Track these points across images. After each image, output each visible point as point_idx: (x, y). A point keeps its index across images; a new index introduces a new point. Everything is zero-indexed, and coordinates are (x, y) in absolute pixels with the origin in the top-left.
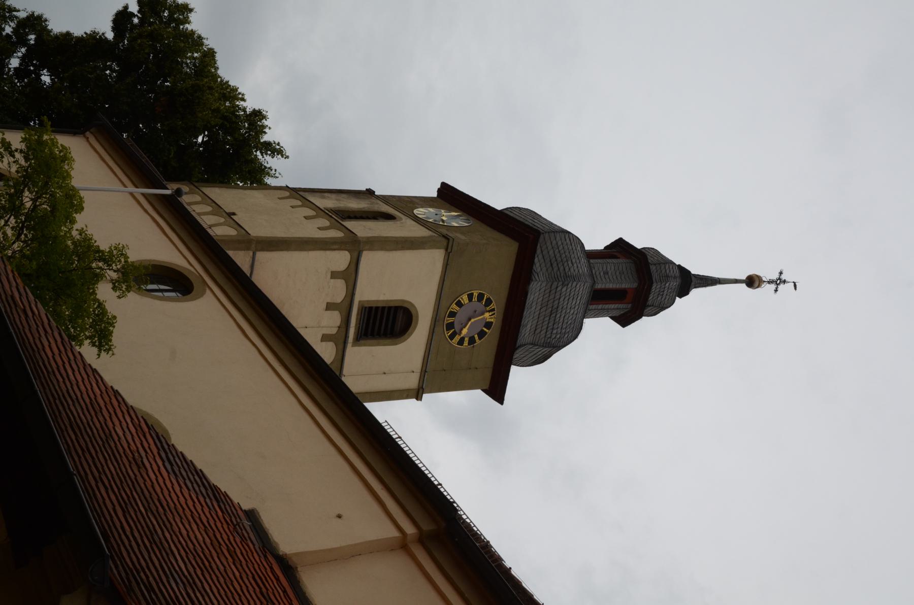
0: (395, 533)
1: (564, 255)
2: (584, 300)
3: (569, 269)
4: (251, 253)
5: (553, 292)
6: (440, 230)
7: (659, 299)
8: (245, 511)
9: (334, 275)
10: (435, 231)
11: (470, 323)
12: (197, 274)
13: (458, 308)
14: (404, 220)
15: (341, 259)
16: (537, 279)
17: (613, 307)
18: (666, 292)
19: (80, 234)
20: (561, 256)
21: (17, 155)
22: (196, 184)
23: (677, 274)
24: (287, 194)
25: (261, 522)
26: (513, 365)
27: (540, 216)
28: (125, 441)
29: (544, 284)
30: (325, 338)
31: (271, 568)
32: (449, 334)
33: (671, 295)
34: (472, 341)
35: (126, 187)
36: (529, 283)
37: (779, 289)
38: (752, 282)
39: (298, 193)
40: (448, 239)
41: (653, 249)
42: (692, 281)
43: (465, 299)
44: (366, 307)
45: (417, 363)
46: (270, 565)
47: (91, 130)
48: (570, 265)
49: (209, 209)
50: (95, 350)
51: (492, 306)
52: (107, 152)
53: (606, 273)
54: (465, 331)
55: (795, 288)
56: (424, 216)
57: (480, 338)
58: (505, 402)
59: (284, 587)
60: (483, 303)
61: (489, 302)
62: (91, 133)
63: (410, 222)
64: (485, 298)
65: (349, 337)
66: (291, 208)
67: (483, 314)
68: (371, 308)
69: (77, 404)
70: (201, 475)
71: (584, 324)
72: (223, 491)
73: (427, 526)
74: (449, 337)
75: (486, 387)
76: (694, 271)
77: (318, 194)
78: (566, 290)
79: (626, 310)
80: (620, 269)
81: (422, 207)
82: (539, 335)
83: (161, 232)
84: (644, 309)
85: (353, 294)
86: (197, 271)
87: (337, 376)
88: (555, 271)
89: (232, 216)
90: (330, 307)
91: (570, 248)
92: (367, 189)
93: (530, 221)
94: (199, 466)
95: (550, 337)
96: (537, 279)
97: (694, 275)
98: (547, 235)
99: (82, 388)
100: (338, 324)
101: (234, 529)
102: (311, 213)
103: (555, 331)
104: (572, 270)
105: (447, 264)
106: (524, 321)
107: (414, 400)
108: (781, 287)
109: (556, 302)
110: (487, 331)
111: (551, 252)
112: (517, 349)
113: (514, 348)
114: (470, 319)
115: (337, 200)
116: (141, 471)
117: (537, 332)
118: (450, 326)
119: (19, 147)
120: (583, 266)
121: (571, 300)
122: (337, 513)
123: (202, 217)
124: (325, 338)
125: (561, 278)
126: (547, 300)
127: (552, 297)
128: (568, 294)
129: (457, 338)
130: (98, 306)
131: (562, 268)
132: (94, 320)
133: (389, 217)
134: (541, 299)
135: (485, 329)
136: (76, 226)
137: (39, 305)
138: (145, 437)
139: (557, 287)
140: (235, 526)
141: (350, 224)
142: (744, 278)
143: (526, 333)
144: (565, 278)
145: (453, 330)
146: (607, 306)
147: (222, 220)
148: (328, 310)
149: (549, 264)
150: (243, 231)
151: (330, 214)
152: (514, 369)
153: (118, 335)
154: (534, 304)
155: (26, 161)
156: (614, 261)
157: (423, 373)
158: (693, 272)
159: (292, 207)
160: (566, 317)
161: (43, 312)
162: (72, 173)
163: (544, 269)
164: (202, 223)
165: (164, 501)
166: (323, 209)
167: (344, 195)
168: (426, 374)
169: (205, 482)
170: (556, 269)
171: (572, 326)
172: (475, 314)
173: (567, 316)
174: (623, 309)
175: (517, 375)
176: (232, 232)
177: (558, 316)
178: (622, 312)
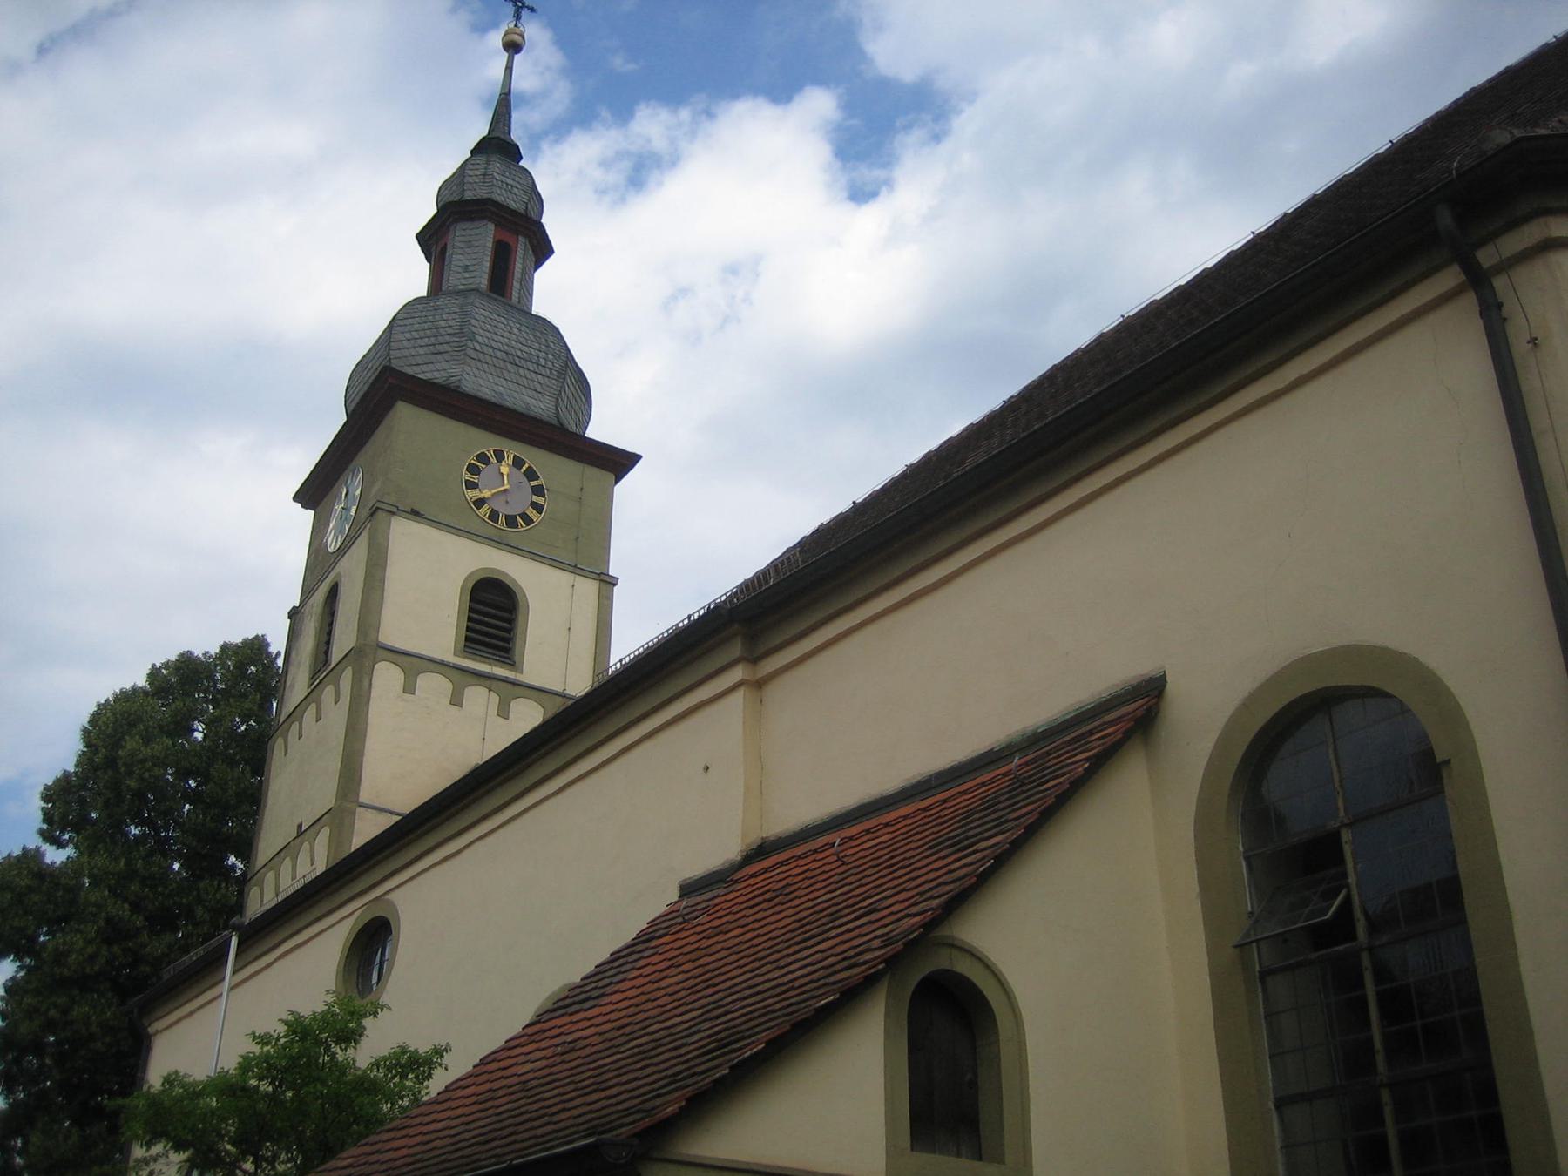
0: (738, 697)
3: (450, 326)
4: (360, 810)
6: (363, 517)
7: (517, 193)
8: (680, 897)
9: (409, 688)
12: (365, 907)
15: (386, 676)
16: (459, 378)
17: (520, 266)
18: (508, 181)
20: (429, 337)
23: (482, 159)
25: (696, 878)
26: (584, 433)
27: (364, 356)
28: (539, 1062)
29: (468, 369)
30: (503, 712)
31: (751, 876)
32: (523, 524)
33: (514, 172)
34: (538, 491)
35: (221, 995)
41: (440, 189)
42: (498, 137)
43: (472, 494)
44: (465, 646)
45: (562, 578)
46: (881, 826)
47: (147, 1024)
49: (288, 862)
52: (181, 1006)
53: (466, 269)
56: (340, 537)
57: (537, 478)
58: (638, 453)
59: (792, 858)
60: (484, 466)
61: (483, 458)
62: (150, 1025)
63: (344, 565)
64: (476, 463)
65: (506, 677)
66: (302, 739)
68: (467, 639)
70: (616, 956)
71: (539, 315)
72: (646, 926)
78: (481, 336)
79: (529, 246)
80: (462, 245)
82: (544, 387)
83: (315, 940)
84: (531, 218)
85: (442, 663)
86: (360, 908)
87: (402, 819)
88: (450, 349)
89: (303, 829)
90: (457, 700)
92: (289, 618)
93: (369, 374)
94: (606, 956)
95: (551, 369)
96: (459, 378)
99: (459, 1112)
100: (484, 691)
101: (689, 923)
102: (310, 713)
103: (543, 362)
104: (452, 323)
106: (520, 407)
107: (615, 588)
110: (527, 465)
111: (421, 351)
112: (561, 424)
113: (562, 429)
116: (578, 1047)
122: (702, 771)
123: (281, 890)
124: (503, 712)
125: (462, 342)
127: (489, 359)
128: (488, 334)
129: (532, 513)
134: (490, 377)
135: (524, 468)
138: (545, 1031)
139: (476, 350)
143: (540, 406)
145: (518, 517)
146: (517, 275)
147: (306, 845)
148: (462, 703)
149: (439, 357)
150: (326, 816)
151: (318, 681)
152: (593, 432)
154: (495, 388)
157: (578, 571)
158: (485, 133)
159: (300, 736)
161: (354, 1151)
163: (445, 365)
164: (289, 892)
165: (622, 1020)
166: (310, 690)
167: (293, 654)
168: (579, 566)
169: (625, 952)
173: (521, 339)
174: (525, 250)
175: (600, 429)
176: (324, 835)
177: (519, 353)
178: (530, 252)
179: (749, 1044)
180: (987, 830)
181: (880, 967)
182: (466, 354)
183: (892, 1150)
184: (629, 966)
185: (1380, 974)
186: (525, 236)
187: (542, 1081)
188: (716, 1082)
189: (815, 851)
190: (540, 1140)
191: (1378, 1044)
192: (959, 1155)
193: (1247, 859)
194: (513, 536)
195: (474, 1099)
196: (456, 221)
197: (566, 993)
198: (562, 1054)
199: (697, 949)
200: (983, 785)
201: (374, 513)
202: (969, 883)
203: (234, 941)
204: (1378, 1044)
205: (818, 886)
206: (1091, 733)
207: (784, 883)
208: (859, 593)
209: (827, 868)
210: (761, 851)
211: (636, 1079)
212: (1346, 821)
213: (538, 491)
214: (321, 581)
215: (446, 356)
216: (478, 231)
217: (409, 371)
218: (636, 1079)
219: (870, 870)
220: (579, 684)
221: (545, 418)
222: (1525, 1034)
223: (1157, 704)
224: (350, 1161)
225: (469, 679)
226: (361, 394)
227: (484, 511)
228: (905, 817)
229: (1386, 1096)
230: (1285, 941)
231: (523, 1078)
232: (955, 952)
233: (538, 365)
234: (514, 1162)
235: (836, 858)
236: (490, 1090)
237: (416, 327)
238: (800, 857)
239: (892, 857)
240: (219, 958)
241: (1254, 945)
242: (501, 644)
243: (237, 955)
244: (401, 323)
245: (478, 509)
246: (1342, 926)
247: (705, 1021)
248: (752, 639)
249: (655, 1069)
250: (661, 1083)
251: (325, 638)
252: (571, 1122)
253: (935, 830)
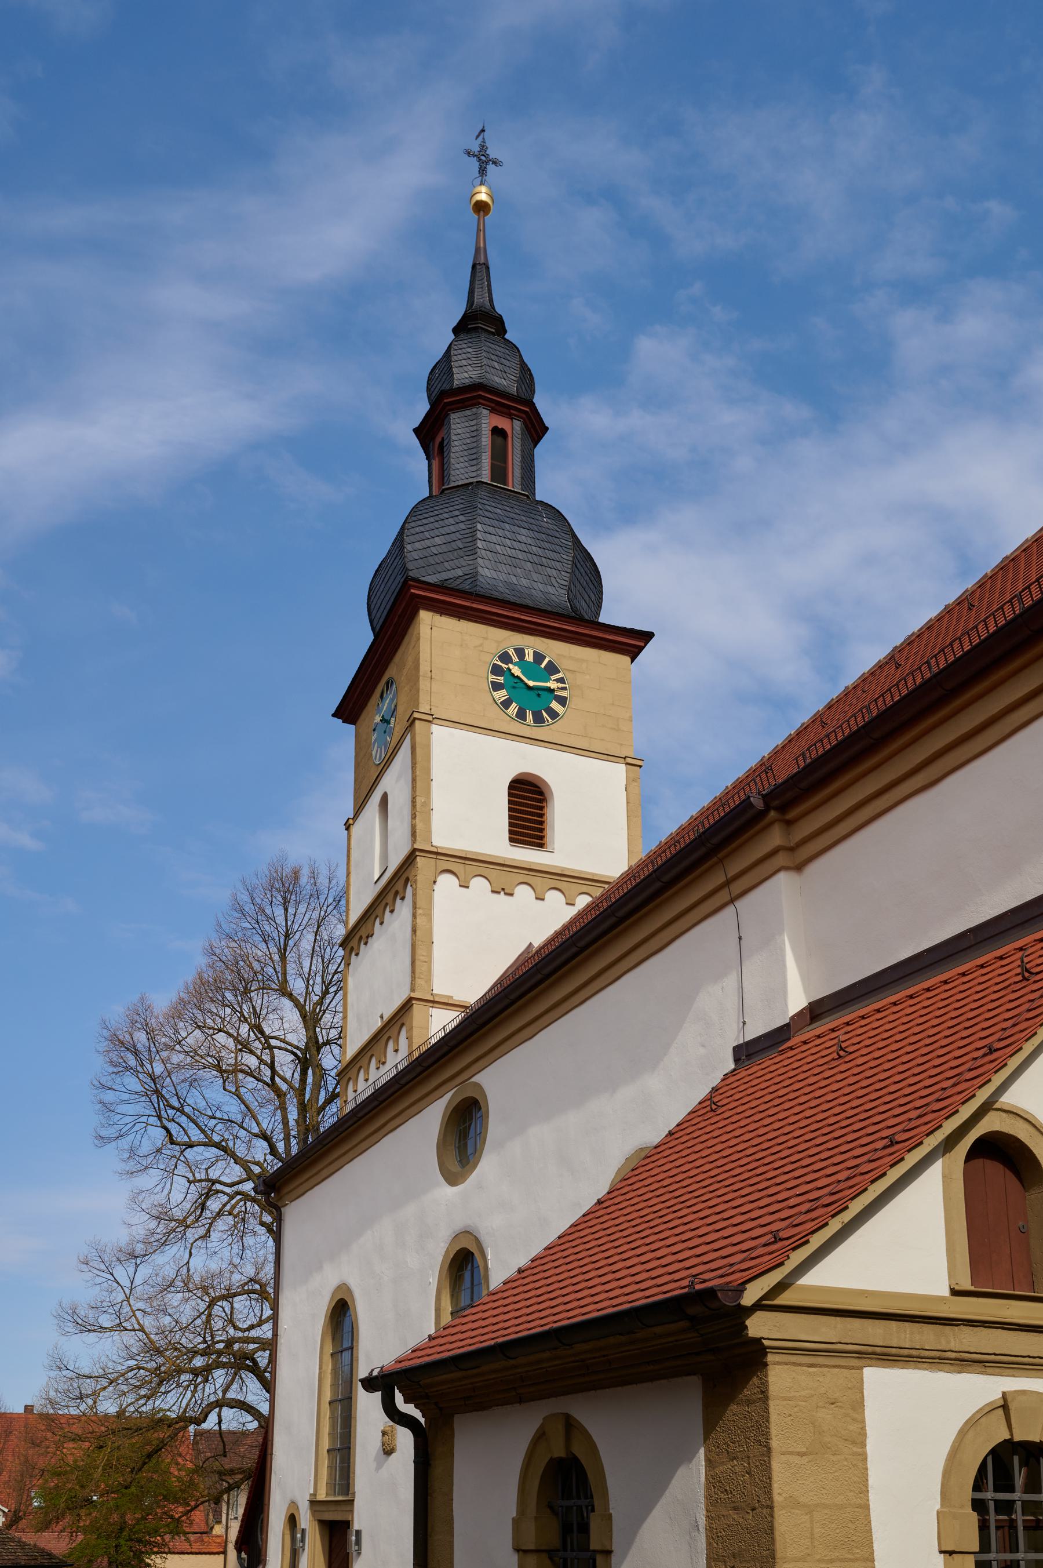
108: (492, 153)
219: (824, 1051)
222: (356, 1408)
245: (507, 709)
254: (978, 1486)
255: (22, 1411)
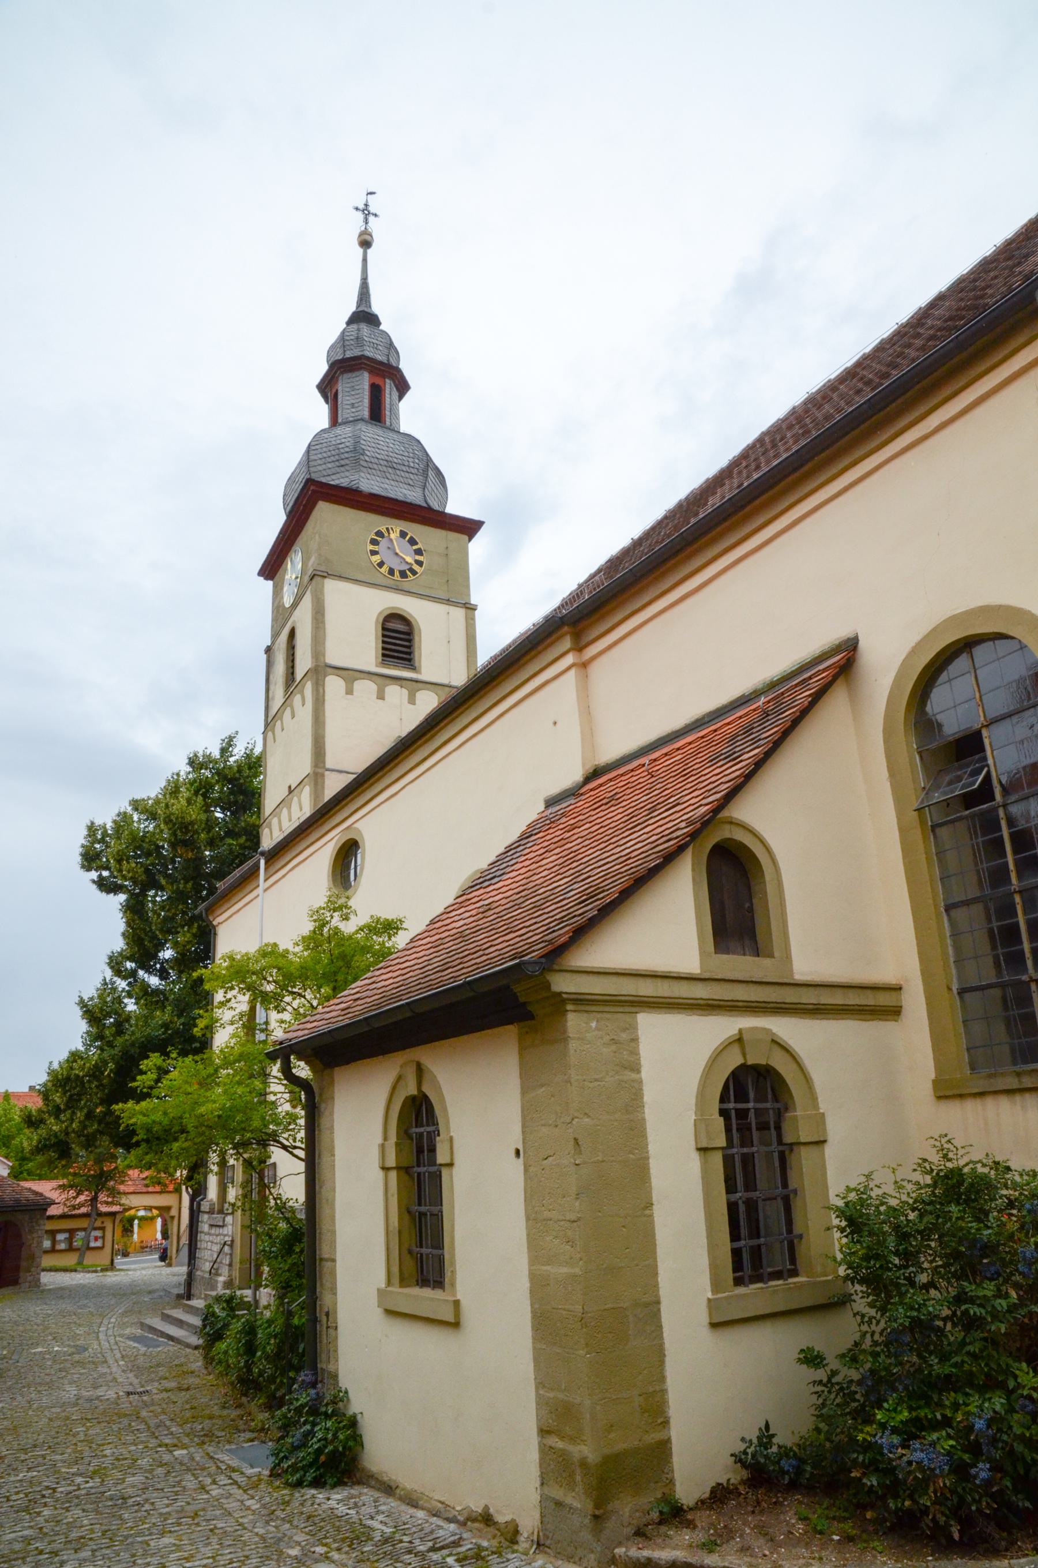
0: (572, 672)
1: (333, 452)
2: (380, 431)
4: (327, 773)
5: (370, 465)
9: (349, 691)
10: (306, 587)
11: (400, 554)
13: (385, 566)
14: (296, 619)
15: (334, 684)
18: (374, 341)
19: (298, 945)
21: (229, 996)
22: (262, 821)
23: (354, 326)
24: (270, 734)
27: (293, 473)
29: (362, 474)
30: (412, 700)
31: (591, 790)
34: (419, 552)
36: (361, 492)
37: (374, 212)
38: (366, 243)
39: (269, 724)
40: (314, 575)
43: (376, 559)
45: (441, 608)
48: (343, 446)
49: (285, 811)
50: (400, 932)
51: (384, 531)
54: (409, 559)
55: (374, 193)
57: (416, 543)
61: (379, 534)
63: (297, 613)
67: (391, 540)
68: (384, 655)
69: (431, 962)
70: (509, 849)
73: (567, 643)
74: (414, 575)
75: (466, 538)
76: (353, 308)
77: (270, 703)
81: (283, 598)
85: (369, 673)
90: (381, 696)
91: (325, 445)
94: (502, 850)
97: (357, 308)
98: (312, 469)
102: (288, 713)
103: (412, 464)
104: (348, 444)
105: (340, 577)
106: (401, 498)
108: (372, 209)
109: (382, 462)
111: (329, 465)
113: (429, 509)
114: (397, 554)
115: (276, 684)
117: (411, 483)
118: (403, 574)
119: (222, 994)
120: (344, 432)
121: (379, 446)
124: (412, 700)
126: (378, 472)
127: (375, 466)
130: (362, 930)
131: (346, 455)
132: (375, 934)
133: (292, 634)
134: (378, 478)
135: (408, 538)
136: (291, 949)
137: (353, 986)
138: (469, 900)
140: (551, 822)
141: (299, 674)
142: (361, 251)
143: (413, 496)
144: (356, 456)
146: (388, 406)
147: (295, 799)
149: (342, 469)
153: (388, 914)
154: (382, 485)
155: (234, 989)
156: (340, 396)
159: (283, 730)
160: (397, 452)
162: (244, 951)
163: (347, 474)
167: (271, 677)
170: (346, 461)
171: (407, 446)
172: (391, 548)
175: (453, 508)
176: (306, 792)
177: (395, 460)
178: (395, 389)
179: (608, 895)
180: (747, 747)
181: (687, 839)
182: (360, 465)
183: (703, 953)
184: (518, 854)
185: (1011, 822)
186: (389, 378)
187: (472, 930)
188: (589, 919)
189: (632, 770)
190: (480, 965)
191: (1011, 866)
192: (744, 954)
193: (920, 753)
194: (406, 584)
195: (429, 946)
196: (342, 373)
197: (480, 875)
198: (483, 913)
199: (562, 839)
200: (740, 717)
201: (315, 577)
202: (739, 782)
203: (262, 862)
204: (1011, 866)
205: (638, 792)
206: (810, 678)
207: (614, 792)
208: (647, 598)
209: (641, 780)
210: (595, 773)
211: (536, 923)
212: (985, 723)
213: (419, 552)
214: (283, 626)
215: (347, 468)
216: (357, 379)
217: (323, 480)
218: (536, 923)
220: (459, 678)
221: (418, 503)
223: (853, 655)
224: (358, 989)
225: (388, 681)
226: (293, 500)
227: (384, 570)
228: (690, 743)
229: (1017, 899)
230: (948, 805)
231: (460, 930)
232: (733, 826)
233: (409, 466)
234: (468, 979)
235: (646, 773)
236: (440, 939)
237: (324, 449)
238: (622, 775)
239: (684, 770)
240: (254, 871)
241: (927, 808)
242: (405, 656)
243: (266, 869)
244: (314, 448)
246: (985, 792)
247: (575, 883)
248: (577, 636)
249: (547, 916)
250: (554, 924)
251: (290, 664)
252: (497, 953)
253: (712, 749)
254: (722, 1100)
255: (27, 1090)
